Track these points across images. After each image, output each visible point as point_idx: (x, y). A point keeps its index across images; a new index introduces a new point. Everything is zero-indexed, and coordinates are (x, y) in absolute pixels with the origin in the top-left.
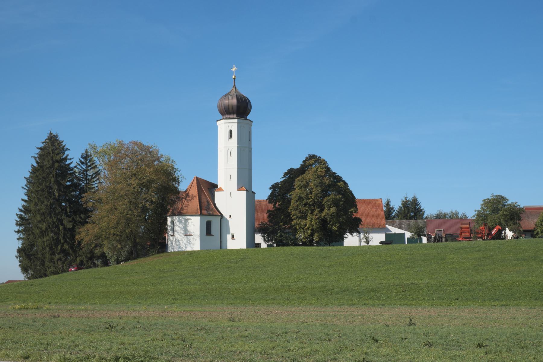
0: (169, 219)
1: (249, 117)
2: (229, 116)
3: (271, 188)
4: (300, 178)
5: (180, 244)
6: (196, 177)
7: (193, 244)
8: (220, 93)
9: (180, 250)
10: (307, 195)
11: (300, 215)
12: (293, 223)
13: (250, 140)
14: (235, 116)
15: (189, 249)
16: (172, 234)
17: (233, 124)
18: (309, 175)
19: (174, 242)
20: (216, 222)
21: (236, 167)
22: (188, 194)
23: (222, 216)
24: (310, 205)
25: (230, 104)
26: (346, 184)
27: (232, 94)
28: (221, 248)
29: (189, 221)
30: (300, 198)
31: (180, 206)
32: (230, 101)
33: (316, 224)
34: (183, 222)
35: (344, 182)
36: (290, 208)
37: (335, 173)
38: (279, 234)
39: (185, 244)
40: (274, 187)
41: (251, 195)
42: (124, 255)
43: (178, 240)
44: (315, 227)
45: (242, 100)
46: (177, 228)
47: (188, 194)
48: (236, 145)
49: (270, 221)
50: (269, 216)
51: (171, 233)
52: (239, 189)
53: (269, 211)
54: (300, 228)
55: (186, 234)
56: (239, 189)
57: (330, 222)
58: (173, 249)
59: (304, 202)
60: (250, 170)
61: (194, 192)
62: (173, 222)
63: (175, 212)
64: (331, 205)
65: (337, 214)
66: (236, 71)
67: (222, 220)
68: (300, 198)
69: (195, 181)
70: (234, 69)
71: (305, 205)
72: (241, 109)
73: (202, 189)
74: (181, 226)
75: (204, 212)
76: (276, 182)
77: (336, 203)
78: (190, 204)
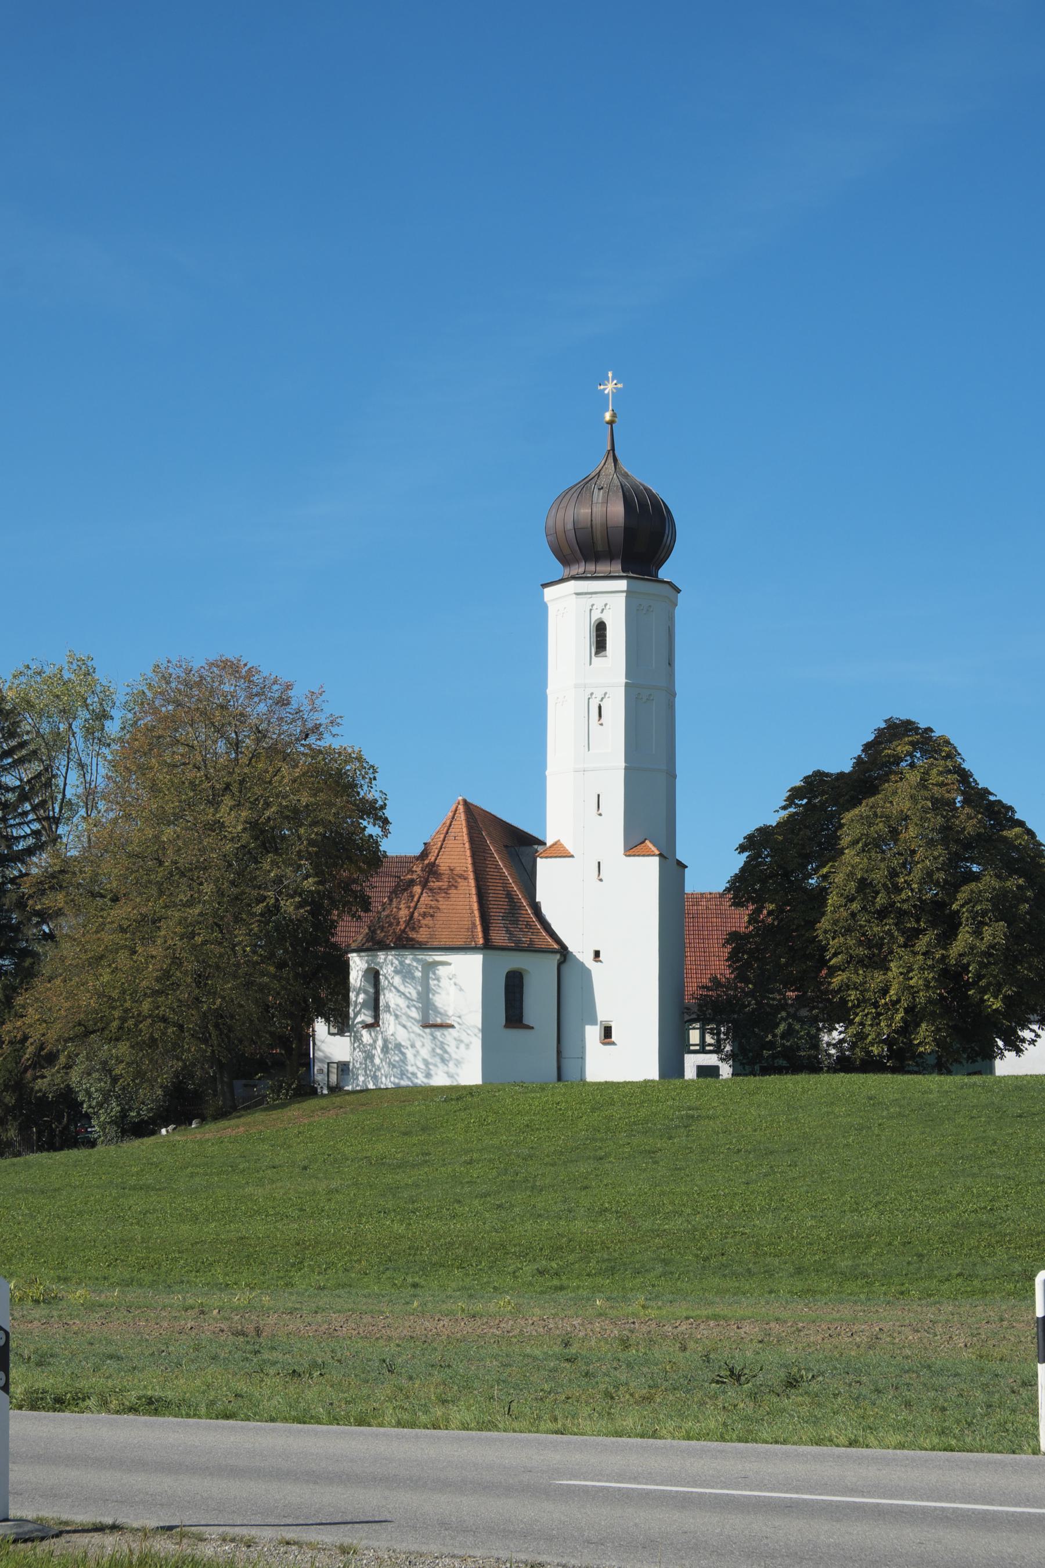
0: (357, 965)
1: (665, 573)
2: (591, 567)
3: (742, 849)
4: (862, 810)
5: (404, 1060)
6: (466, 803)
7: (458, 1063)
8: (552, 479)
9: (404, 1083)
10: (893, 874)
11: (862, 951)
12: (836, 981)
13: (671, 663)
14: (617, 567)
15: (440, 1080)
16: (370, 1020)
17: (609, 597)
18: (899, 796)
19: (378, 1052)
20: (540, 974)
21: (621, 764)
22: (433, 864)
23: (563, 951)
24: (902, 914)
25: (598, 520)
26: (1031, 833)
27: (603, 481)
28: (559, 1078)
29: (442, 971)
30: (864, 885)
31: (404, 913)
32: (598, 510)
33: (927, 987)
34: (418, 974)
35: (1021, 824)
36: (824, 924)
37: (987, 792)
38: (782, 1027)
39: (426, 1063)
40: (756, 842)
41: (673, 871)
42: (149, 1098)
43: (398, 1046)
44: (922, 997)
45: (643, 505)
46: (389, 998)
47: (433, 864)
48: (622, 680)
49: (742, 977)
50: (733, 957)
51: (366, 1017)
52: (633, 847)
53: (734, 937)
54: (861, 1002)
55: (423, 1024)
56: (633, 847)
57: (979, 977)
58: (375, 1078)
59: (881, 900)
60: (672, 776)
61: (457, 857)
62: (373, 976)
63: (380, 935)
64: (984, 913)
65: (1007, 948)
66: (617, 393)
67: (565, 968)
68: (864, 885)
69: (462, 817)
70: (609, 388)
71: (882, 914)
72: (636, 542)
73: (486, 850)
74: (412, 991)
75: (499, 937)
76: (760, 824)
77: (1003, 907)
78: (443, 904)
